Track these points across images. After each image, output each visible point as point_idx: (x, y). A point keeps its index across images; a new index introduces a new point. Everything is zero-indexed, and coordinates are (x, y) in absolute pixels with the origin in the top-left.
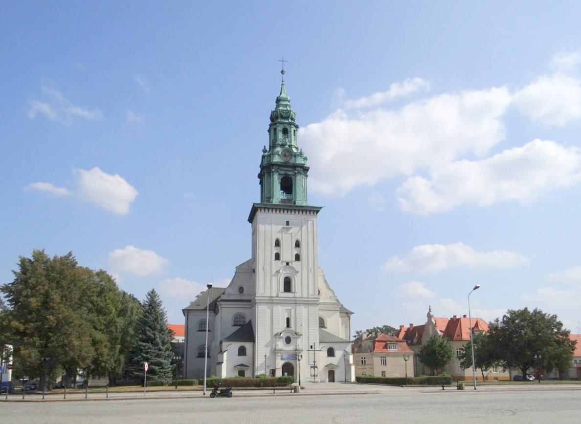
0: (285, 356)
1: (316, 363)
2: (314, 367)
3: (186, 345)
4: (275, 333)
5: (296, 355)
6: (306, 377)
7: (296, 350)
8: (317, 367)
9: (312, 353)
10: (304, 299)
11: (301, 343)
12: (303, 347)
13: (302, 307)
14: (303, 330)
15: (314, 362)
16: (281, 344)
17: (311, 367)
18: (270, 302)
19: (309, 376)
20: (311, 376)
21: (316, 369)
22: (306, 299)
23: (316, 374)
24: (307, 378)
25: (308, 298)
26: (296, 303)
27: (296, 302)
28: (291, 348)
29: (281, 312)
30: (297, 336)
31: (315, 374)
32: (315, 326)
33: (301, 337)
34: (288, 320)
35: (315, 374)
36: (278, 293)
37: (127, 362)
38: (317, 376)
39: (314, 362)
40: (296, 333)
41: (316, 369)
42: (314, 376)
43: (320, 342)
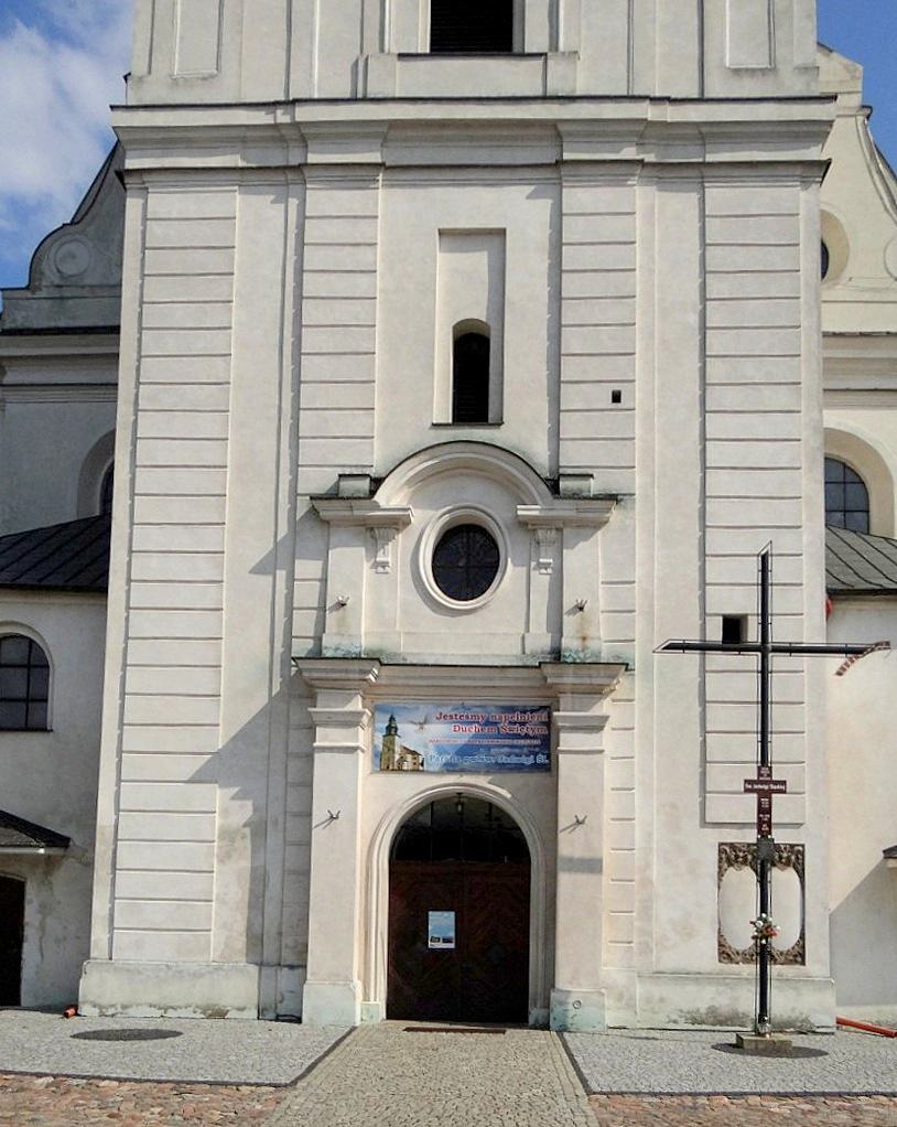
0: (428, 735)
1: (781, 807)
2: (764, 856)
3: (742, 645)
4: (317, 480)
5: (532, 714)
6: (670, 960)
7: (557, 655)
8: (795, 858)
9: (735, 675)
10: (650, 112)
11: (622, 585)
12: (233, 1023)
13: (641, 195)
14: (644, 450)
15: (765, 787)
16: (382, 597)
17: (730, 856)
18: (276, 158)
19: (705, 954)
20: (725, 954)
21: (782, 878)
22: (671, 114)
23: (783, 941)
24: (682, 976)
25: (701, 100)
26: (560, 163)
27: (548, 151)
28: (500, 627)
29: (403, 260)
30: (564, 509)
31: (766, 933)
32: (782, 398)
33: (615, 515)
34: (474, 356)
35: (766, 933)
36: (359, 69)
37: (589, 643)
38: (798, 956)
39: (765, 787)
40: (553, 486)
41: (782, 878)
42: (763, 955)
43: (835, 595)
